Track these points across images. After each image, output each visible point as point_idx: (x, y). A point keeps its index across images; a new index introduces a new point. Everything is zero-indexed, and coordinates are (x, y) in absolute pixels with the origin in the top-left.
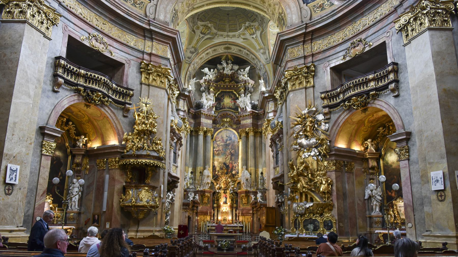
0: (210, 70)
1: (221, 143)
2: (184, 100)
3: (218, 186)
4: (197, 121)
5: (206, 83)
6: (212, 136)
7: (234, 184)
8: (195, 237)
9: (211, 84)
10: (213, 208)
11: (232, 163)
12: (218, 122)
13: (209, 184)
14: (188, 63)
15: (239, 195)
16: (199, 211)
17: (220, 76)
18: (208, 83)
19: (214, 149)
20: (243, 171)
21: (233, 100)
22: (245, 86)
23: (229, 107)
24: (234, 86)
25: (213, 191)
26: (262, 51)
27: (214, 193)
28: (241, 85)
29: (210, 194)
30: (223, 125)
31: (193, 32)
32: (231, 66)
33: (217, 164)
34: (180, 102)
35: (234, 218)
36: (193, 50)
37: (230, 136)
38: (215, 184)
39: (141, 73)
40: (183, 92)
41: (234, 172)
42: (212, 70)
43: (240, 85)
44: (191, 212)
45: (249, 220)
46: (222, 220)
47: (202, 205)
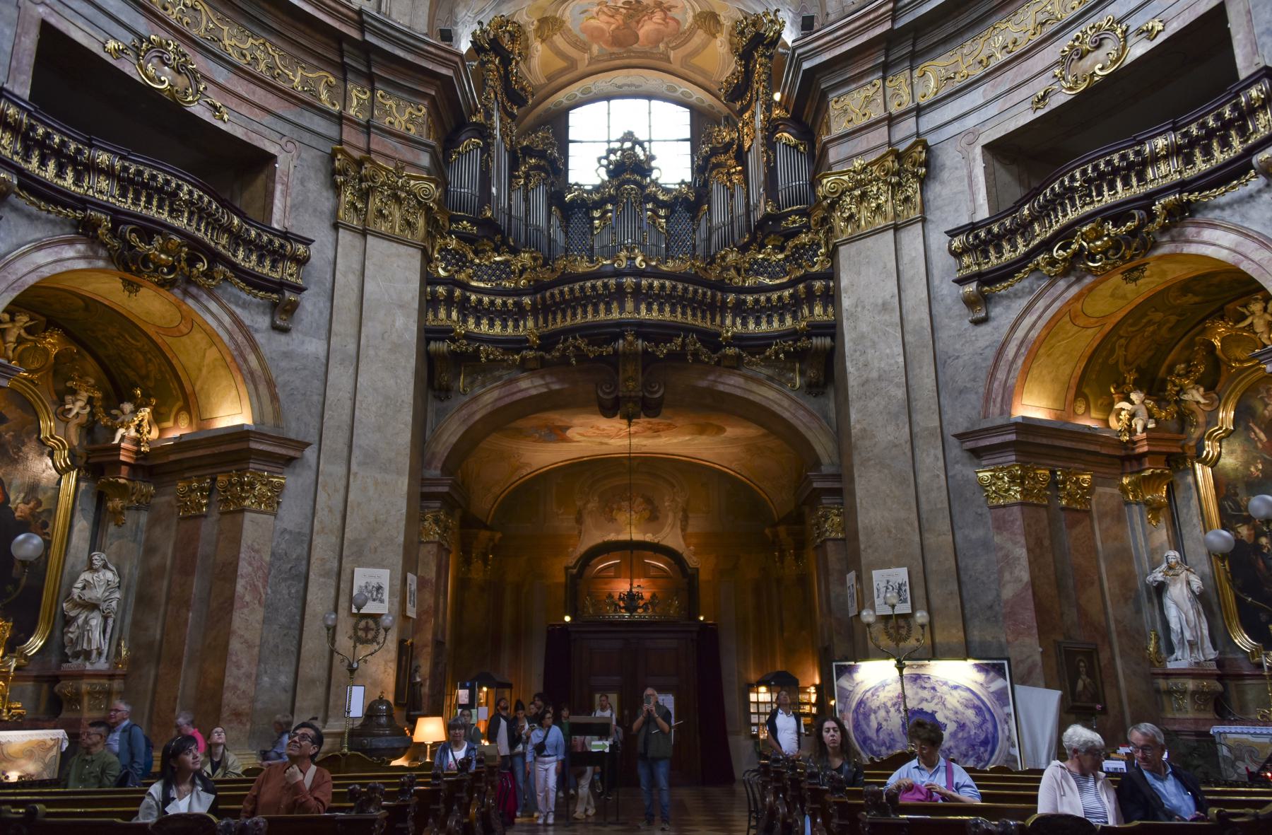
39: (336, 189)
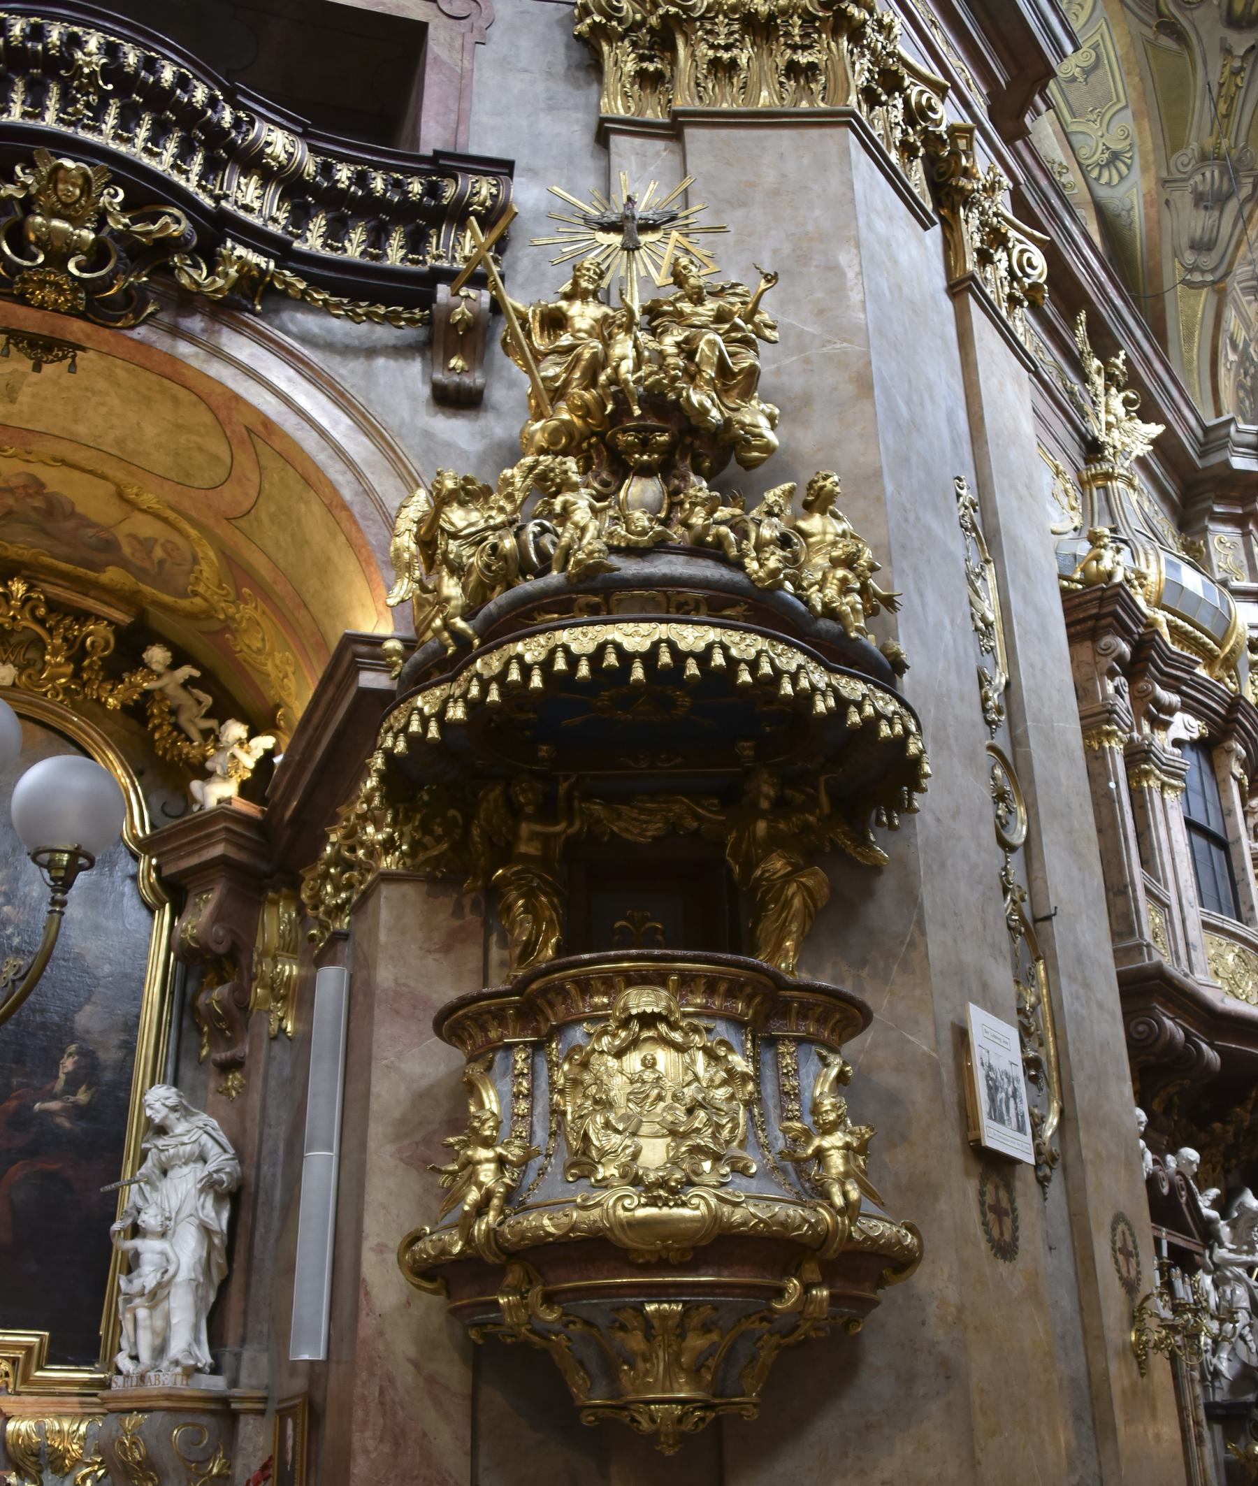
2: (1239, 522)
14: (1202, 285)
31: (1165, 41)
34: (1214, 541)
40: (1215, 459)
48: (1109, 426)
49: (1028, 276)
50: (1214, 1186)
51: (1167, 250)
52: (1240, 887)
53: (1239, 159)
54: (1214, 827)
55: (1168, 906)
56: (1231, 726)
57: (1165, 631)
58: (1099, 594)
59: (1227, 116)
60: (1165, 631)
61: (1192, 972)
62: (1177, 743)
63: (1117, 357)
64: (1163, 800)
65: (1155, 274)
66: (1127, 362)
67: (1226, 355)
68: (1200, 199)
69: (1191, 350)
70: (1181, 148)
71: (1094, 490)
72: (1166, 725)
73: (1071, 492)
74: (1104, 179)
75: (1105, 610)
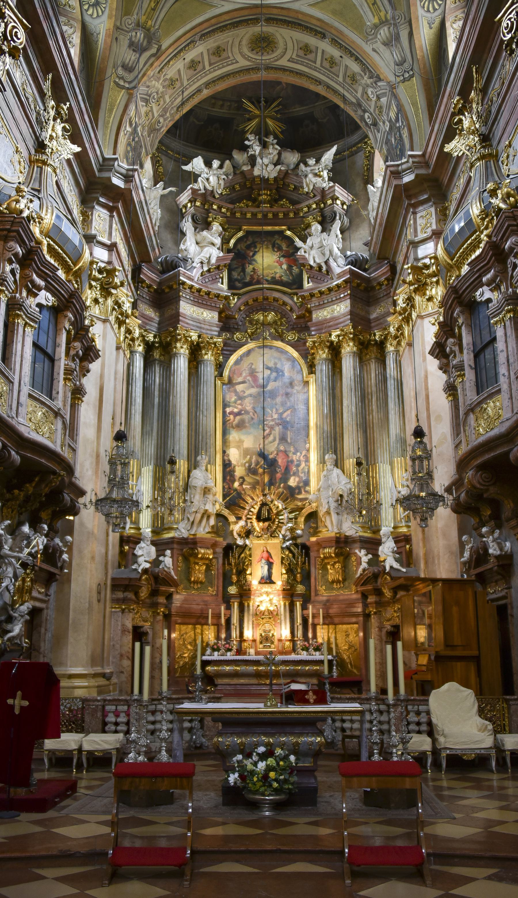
0: (208, 164)
1: (248, 388)
2: (111, 209)
3: (242, 523)
4: (169, 312)
5: (198, 204)
6: (220, 367)
7: (296, 518)
8: (128, 715)
9: (215, 207)
10: (227, 600)
11: (286, 453)
12: (237, 324)
13: (209, 517)
14: (123, 87)
15: (312, 554)
16: (173, 610)
17: (243, 186)
18: (203, 204)
19: (228, 410)
20: (325, 473)
21: (283, 256)
22: (321, 210)
23: (273, 278)
24: (286, 215)
25: (223, 542)
26: (384, 32)
27: (229, 549)
28: (309, 207)
29: (214, 553)
30: (253, 337)
32: (276, 152)
33: (237, 456)
34: (96, 214)
35: (299, 633)
36: (140, 36)
37: (279, 366)
38: (232, 519)
40: (105, 175)
41: (293, 482)
42: (216, 163)
43: (305, 209)
44: (146, 614)
45: (351, 638)
46: (258, 638)
47: (185, 588)
48: (51, 138)
49: (14, 42)
50: (7, 520)
51: (111, 64)
52: (55, 382)
53: (154, 34)
54: (49, 350)
55: (12, 383)
56: (69, 304)
57: (45, 249)
58: (12, 219)
59: (154, 9)
60: (45, 249)
61: (17, 417)
62: (39, 305)
63: (65, 105)
64: (24, 331)
65: (103, 71)
66: (70, 109)
67: (126, 127)
68: (132, 45)
69: (110, 117)
70: (129, 15)
71: (36, 167)
72: (35, 295)
73: (22, 163)
74: (90, 12)
75: (14, 228)
